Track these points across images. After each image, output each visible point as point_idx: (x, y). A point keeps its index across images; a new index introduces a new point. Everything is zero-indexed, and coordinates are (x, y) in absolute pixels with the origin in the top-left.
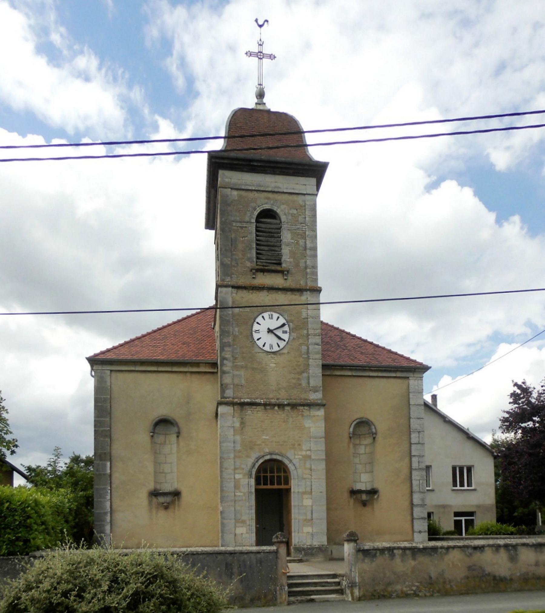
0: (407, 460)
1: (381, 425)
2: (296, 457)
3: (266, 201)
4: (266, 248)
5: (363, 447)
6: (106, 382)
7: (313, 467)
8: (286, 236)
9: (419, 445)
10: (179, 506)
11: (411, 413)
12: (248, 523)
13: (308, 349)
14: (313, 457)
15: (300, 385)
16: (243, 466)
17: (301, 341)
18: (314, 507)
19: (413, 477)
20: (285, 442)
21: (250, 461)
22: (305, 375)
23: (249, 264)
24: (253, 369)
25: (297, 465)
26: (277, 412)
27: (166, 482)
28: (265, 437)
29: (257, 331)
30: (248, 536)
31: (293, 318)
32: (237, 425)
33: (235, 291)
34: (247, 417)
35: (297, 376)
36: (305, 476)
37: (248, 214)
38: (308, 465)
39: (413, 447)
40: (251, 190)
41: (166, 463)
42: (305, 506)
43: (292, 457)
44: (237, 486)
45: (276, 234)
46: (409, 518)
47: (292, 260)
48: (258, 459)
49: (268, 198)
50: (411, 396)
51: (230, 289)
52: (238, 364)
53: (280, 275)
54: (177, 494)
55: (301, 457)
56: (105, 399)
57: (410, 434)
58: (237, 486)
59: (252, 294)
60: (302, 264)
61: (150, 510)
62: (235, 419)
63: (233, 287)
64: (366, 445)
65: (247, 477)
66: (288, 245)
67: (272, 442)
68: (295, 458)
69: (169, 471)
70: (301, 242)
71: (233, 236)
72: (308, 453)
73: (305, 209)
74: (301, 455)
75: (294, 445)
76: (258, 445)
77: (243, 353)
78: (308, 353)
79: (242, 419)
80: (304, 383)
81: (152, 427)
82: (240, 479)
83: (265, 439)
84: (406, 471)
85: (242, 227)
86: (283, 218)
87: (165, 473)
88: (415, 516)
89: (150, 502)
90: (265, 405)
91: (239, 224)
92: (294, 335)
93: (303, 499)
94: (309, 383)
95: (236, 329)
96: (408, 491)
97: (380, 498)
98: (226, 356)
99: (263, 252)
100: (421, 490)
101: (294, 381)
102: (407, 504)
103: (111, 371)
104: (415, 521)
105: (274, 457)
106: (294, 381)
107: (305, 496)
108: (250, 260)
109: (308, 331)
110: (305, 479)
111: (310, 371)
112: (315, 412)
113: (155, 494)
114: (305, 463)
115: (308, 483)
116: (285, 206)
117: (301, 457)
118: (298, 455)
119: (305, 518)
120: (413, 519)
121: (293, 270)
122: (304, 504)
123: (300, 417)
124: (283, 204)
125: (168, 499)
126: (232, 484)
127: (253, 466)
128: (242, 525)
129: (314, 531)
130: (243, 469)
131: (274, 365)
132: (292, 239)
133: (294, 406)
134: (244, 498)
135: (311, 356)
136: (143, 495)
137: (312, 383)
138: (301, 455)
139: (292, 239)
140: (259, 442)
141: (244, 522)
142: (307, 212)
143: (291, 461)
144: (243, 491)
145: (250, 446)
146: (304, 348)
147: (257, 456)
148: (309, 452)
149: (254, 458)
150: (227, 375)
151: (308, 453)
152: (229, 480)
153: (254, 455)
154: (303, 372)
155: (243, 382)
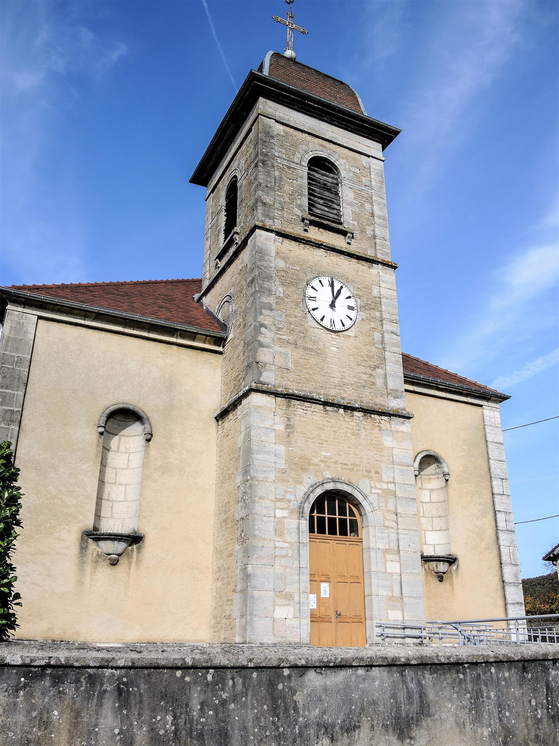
0: (491, 516)
1: (452, 461)
2: (374, 491)
3: (321, 148)
4: (321, 202)
5: (427, 493)
6: (26, 332)
7: (399, 510)
8: (346, 193)
9: (504, 497)
10: (138, 561)
11: (490, 452)
12: (297, 599)
13: (383, 337)
14: (399, 494)
15: (374, 384)
16: (288, 496)
17: (373, 325)
18: (403, 576)
19: (501, 542)
20: (355, 465)
21: (302, 490)
22: (379, 371)
23: (299, 213)
24: (305, 349)
25: (375, 504)
26: (344, 418)
27: (112, 517)
28: (325, 454)
29: (313, 299)
30: (296, 622)
31: (360, 293)
32: (281, 427)
33: (280, 239)
34: (297, 418)
35: (368, 371)
36: (388, 524)
37: (298, 155)
38: (391, 507)
39: (497, 499)
40: (303, 131)
41: (115, 483)
42: (390, 573)
43: (366, 491)
44: (279, 532)
45: (333, 190)
46: (501, 602)
47: (356, 223)
48: (314, 487)
49: (324, 147)
50: (488, 429)
51: (273, 235)
52: (283, 337)
53: (342, 237)
54: (135, 539)
55: (380, 491)
56: (20, 361)
57: (491, 481)
58: (279, 532)
59: (304, 249)
60: (369, 230)
61: (82, 563)
62: (277, 418)
63: (279, 234)
64: (431, 490)
65: (296, 516)
66: (351, 204)
67: (336, 462)
68: (371, 493)
69: (121, 498)
70: (367, 206)
71: (277, 173)
72: (391, 487)
73: (370, 172)
74: (380, 489)
75: (370, 472)
76: (312, 464)
77: (291, 324)
78: (383, 342)
79: (289, 419)
80: (379, 382)
81: (104, 419)
82: (284, 518)
83: (326, 457)
84: (490, 532)
85: (289, 168)
86: (343, 173)
87: (113, 501)
88: (509, 600)
89: (83, 549)
90: (325, 404)
91: (285, 163)
92: (362, 315)
93: (386, 561)
94: (386, 384)
95: (281, 289)
96: (496, 562)
97: (460, 570)
98: (266, 322)
99: (318, 206)
100: (513, 563)
101: (365, 377)
102: (496, 581)
103: (40, 318)
104: (508, 606)
105: (340, 487)
106: (365, 377)
107: (389, 557)
108: (300, 207)
109: (381, 314)
110: (387, 527)
111: (388, 368)
112: (398, 427)
113: (94, 535)
114: (387, 503)
115: (393, 536)
116: (345, 161)
117: (380, 491)
118: (376, 488)
119: (390, 594)
120: (506, 604)
121: (357, 235)
122: (389, 570)
123: (376, 430)
124: (343, 158)
125: (120, 546)
126: (271, 527)
127: (307, 496)
128: (286, 602)
129: (406, 618)
130: (290, 501)
131: (336, 350)
132: (355, 199)
133: (367, 412)
134: (290, 552)
135: (388, 348)
136: (71, 537)
137: (391, 384)
138: (380, 489)
139: (355, 199)
140: (316, 461)
141: (289, 597)
142: (372, 176)
143: (365, 497)
144: (289, 540)
145: (299, 465)
146: (377, 336)
147: (313, 483)
148: (393, 485)
149: (308, 486)
150: (265, 349)
151: (391, 487)
152: (264, 518)
153: (309, 480)
154: (376, 367)
155: (290, 365)
